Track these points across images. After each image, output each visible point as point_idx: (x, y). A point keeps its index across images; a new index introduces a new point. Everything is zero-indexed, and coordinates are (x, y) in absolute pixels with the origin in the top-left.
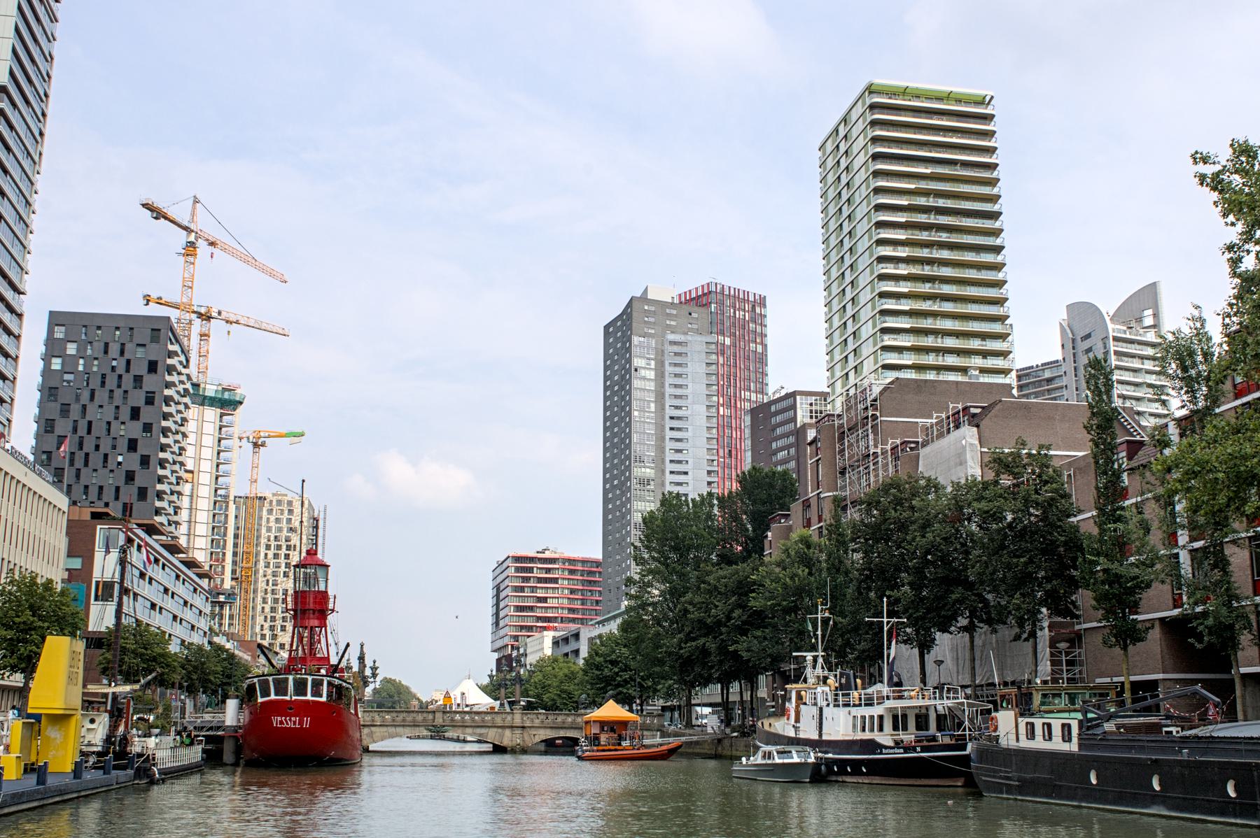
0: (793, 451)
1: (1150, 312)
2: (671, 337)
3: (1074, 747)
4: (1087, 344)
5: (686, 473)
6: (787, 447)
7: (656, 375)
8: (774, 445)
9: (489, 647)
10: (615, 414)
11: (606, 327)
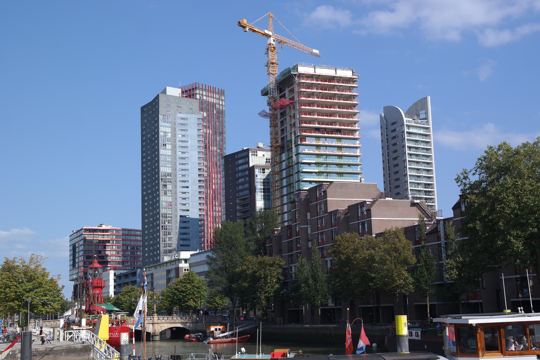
0: (247, 179)
1: (424, 111)
2: (179, 115)
3: (419, 338)
4: (394, 141)
5: (188, 187)
6: (245, 177)
7: (172, 147)
8: (237, 175)
9: (68, 278)
10: (149, 189)
11: (142, 108)
